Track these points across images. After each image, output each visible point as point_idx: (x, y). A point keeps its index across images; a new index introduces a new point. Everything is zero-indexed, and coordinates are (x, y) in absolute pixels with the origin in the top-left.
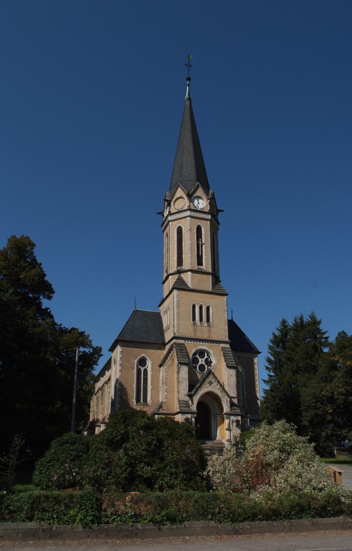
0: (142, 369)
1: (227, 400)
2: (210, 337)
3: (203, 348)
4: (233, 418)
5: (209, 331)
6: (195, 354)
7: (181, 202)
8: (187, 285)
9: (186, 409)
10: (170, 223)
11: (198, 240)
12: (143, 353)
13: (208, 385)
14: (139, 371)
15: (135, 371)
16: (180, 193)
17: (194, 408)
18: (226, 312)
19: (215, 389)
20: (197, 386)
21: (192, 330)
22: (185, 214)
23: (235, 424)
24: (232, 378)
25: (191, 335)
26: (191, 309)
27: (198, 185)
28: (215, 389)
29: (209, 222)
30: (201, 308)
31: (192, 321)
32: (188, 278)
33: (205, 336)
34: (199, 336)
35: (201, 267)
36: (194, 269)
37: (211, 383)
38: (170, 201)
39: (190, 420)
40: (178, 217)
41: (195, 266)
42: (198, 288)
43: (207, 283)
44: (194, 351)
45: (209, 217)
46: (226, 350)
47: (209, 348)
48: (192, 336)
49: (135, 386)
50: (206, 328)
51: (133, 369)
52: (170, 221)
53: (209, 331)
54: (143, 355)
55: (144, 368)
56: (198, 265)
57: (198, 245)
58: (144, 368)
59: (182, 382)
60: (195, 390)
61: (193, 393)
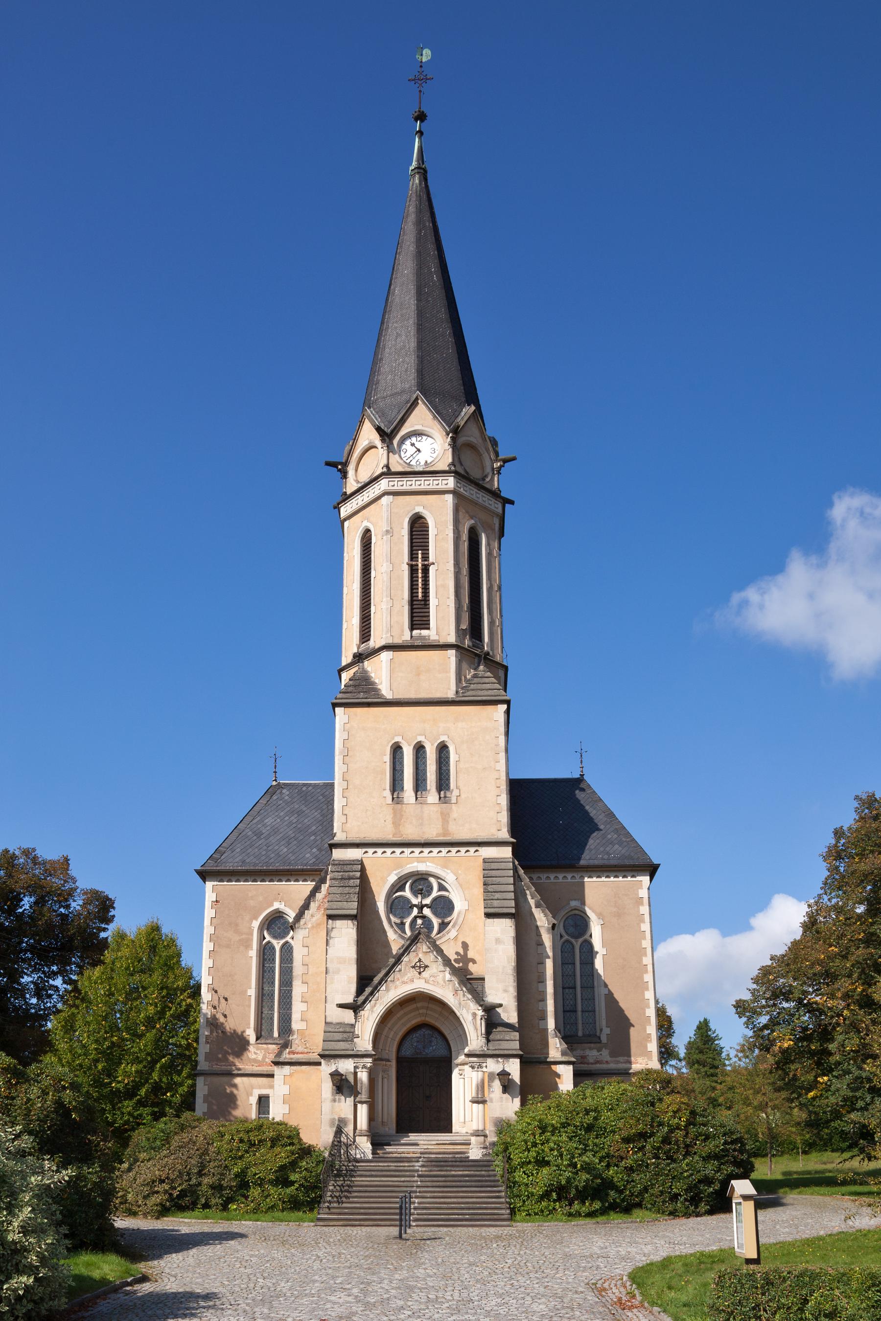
0: (577, 944)
1: (474, 1015)
2: (446, 832)
3: (422, 867)
4: (493, 1066)
5: (445, 818)
6: (399, 885)
7: (369, 458)
8: (377, 690)
9: (342, 1045)
10: (346, 524)
11: (413, 556)
12: (276, 900)
13: (414, 973)
14: (265, 953)
15: (253, 953)
16: (368, 434)
17: (365, 1042)
18: (502, 755)
19: (439, 984)
20: (376, 980)
21: (389, 818)
22: (399, 484)
23: (497, 1085)
24: (501, 947)
25: (385, 831)
26: (387, 758)
27: (417, 399)
28: (435, 983)
29: (449, 498)
30: (419, 749)
31: (388, 794)
32: (380, 670)
33: (432, 833)
34: (410, 833)
35: (424, 632)
36: (398, 641)
37: (421, 967)
38: (346, 464)
39: (351, 1079)
40: (415, 487)
41: (402, 634)
42: (412, 695)
43: (441, 672)
44: (392, 878)
45: (450, 482)
46: (494, 866)
47: (445, 866)
48: (390, 838)
49: (252, 992)
50: (435, 809)
51: (248, 946)
52: (345, 520)
53: (445, 818)
54: (276, 905)
55: (282, 942)
56: (412, 628)
57: (413, 570)
58: (282, 942)
59: (338, 972)
60: (368, 990)
61: (362, 998)
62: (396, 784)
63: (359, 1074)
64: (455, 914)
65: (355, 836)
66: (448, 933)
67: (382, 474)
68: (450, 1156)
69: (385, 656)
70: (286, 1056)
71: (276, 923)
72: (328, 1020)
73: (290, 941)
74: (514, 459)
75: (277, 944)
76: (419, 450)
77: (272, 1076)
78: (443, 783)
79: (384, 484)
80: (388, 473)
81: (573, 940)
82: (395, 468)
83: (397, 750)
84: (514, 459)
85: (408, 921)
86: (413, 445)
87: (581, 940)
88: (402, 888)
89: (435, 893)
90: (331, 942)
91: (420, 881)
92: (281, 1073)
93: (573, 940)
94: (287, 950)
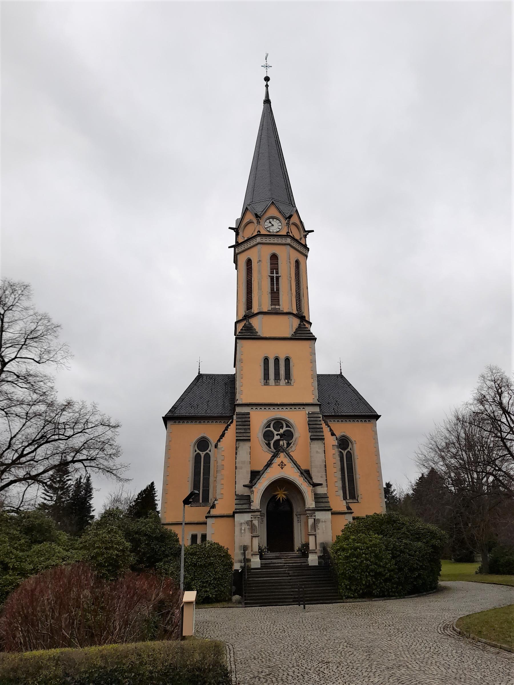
0: (345, 453)
9: (245, 506)
30: (277, 360)
35: (277, 307)
37: (282, 465)
52: (238, 254)
55: (205, 453)
57: (272, 278)
58: (205, 453)
59: (241, 468)
62: (266, 376)
63: (254, 522)
64: (294, 439)
65: (244, 402)
66: (291, 447)
67: (257, 235)
68: (300, 564)
69: (260, 316)
70: (213, 512)
71: (203, 444)
72: (237, 493)
73: (209, 452)
74: (313, 231)
75: (203, 454)
76: (273, 225)
77: (206, 523)
78: (288, 376)
79: (258, 240)
80: (259, 235)
81: (343, 451)
82: (263, 232)
83: (266, 360)
84: (313, 231)
85: (272, 442)
86: (270, 222)
87: (346, 451)
88: (269, 426)
89: (285, 428)
90: (238, 453)
91: (278, 423)
92: (210, 521)
93: (343, 451)
94: (207, 457)
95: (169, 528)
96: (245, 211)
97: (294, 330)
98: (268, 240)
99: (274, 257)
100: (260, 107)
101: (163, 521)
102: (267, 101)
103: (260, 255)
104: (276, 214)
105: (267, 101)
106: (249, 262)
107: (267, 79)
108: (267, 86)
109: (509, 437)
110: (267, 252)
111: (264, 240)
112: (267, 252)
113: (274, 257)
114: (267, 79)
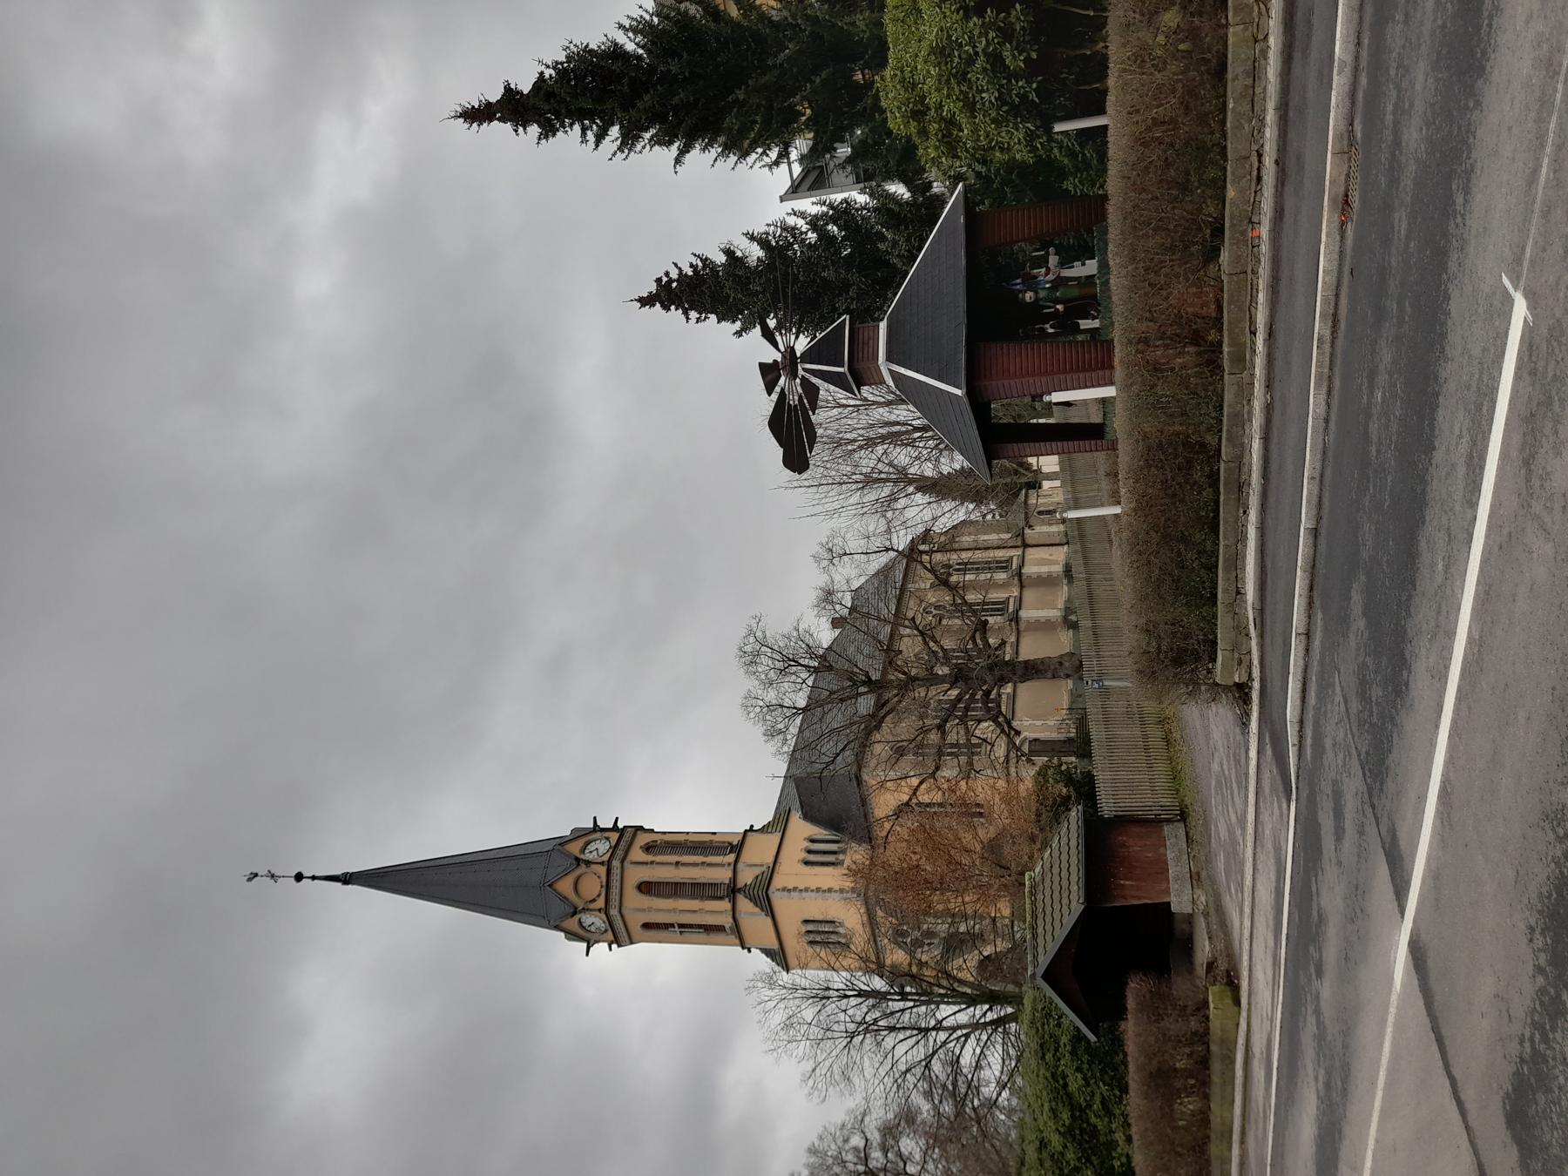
30: (809, 852)
79: (614, 912)
83: (807, 863)
95: (956, 1008)
96: (557, 928)
97: (757, 910)
98: (615, 891)
99: (646, 888)
100: (499, 130)
101: (1022, 687)
102: (346, 879)
103: (638, 907)
104: (570, 880)
105: (346, 879)
106: (646, 926)
107: (299, 877)
108: (314, 878)
109: (931, 1040)
110: (634, 899)
111: (615, 901)
112: (634, 899)
113: (646, 888)
114: (299, 877)
